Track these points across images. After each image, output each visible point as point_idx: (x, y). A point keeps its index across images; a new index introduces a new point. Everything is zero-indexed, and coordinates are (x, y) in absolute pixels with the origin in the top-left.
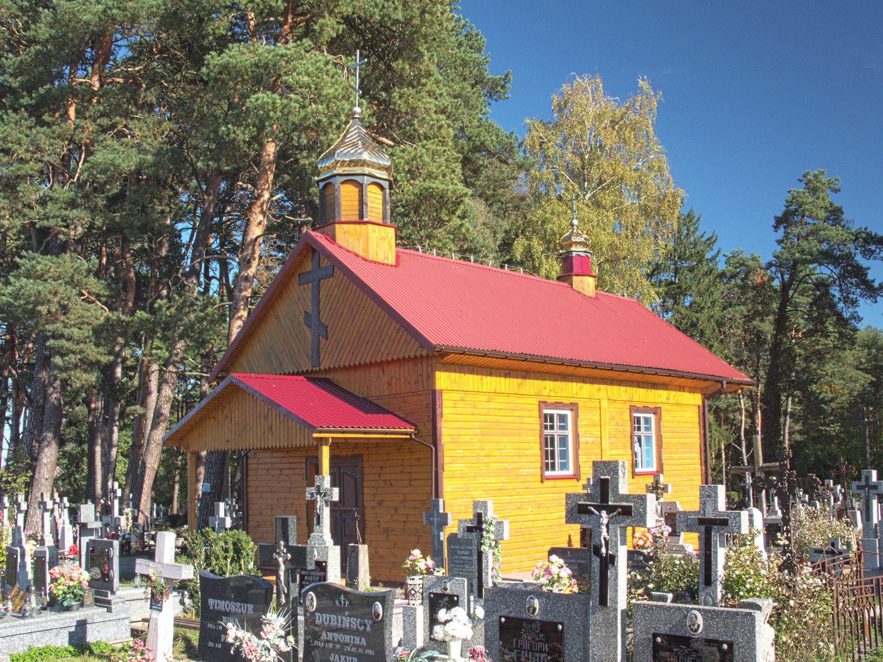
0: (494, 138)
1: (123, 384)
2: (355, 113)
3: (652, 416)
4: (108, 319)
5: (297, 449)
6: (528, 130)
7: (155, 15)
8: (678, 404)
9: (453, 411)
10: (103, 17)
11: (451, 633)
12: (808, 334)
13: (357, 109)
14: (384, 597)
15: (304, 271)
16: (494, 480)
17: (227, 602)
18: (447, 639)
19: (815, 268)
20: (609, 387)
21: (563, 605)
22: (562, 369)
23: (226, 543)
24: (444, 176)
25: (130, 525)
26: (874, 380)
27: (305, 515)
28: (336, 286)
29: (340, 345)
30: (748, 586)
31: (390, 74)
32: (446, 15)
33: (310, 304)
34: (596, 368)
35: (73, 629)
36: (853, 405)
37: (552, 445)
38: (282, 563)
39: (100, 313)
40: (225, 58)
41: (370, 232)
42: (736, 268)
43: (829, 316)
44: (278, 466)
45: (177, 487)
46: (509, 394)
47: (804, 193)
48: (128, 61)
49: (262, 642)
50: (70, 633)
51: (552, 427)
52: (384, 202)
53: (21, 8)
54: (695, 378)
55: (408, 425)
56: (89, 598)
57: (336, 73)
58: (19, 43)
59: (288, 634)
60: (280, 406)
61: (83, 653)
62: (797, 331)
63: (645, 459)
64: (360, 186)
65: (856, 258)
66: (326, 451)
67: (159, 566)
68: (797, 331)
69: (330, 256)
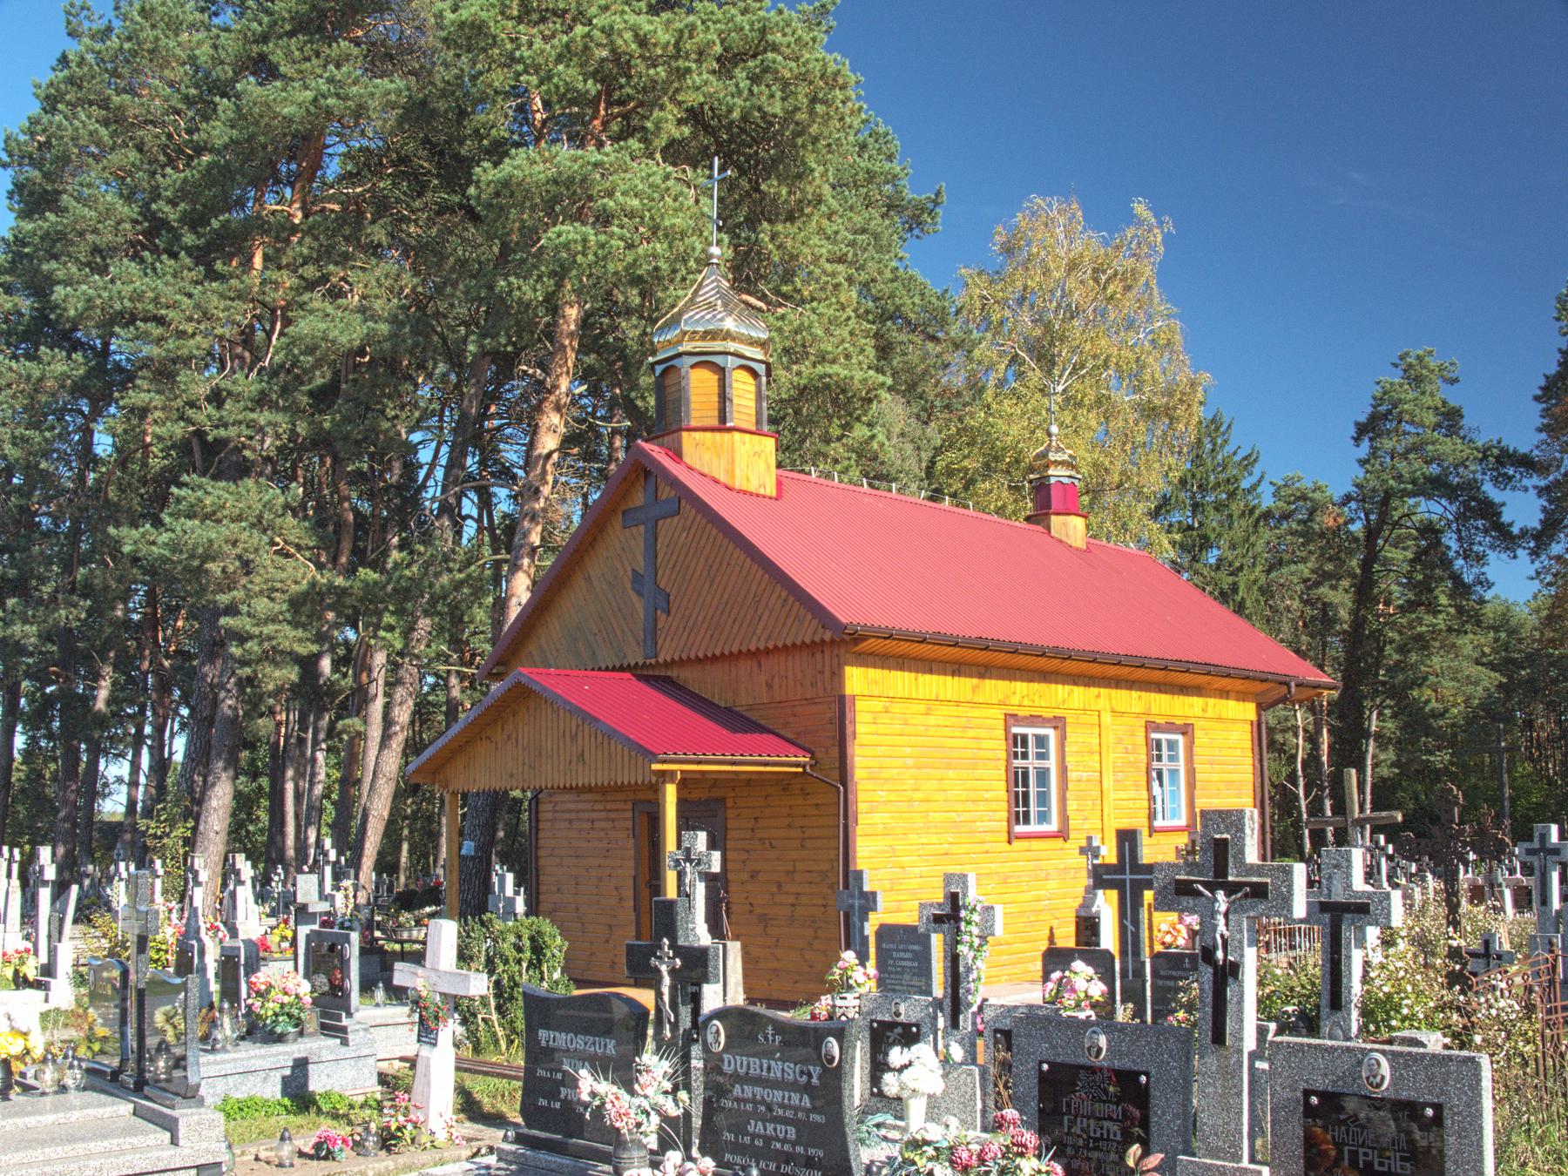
0: (917, 300)
1: (332, 683)
2: (711, 256)
3: (1180, 738)
4: (313, 584)
5: (620, 788)
6: (968, 288)
7: (394, 106)
8: (1219, 719)
9: (873, 728)
10: (312, 109)
11: (912, 1085)
12: (1409, 607)
13: (715, 250)
14: (843, 1029)
15: (631, 505)
16: (934, 839)
17: (571, 1035)
18: (905, 1095)
19: (1417, 505)
20: (1114, 692)
21: (1148, 1043)
22: (1042, 663)
23: (519, 937)
24: (848, 357)
25: (351, 906)
26: (1505, 680)
27: (631, 893)
28: (683, 529)
29: (690, 624)
30: (1405, 1011)
31: (756, 196)
32: (849, 104)
33: (641, 559)
34: (1094, 661)
35: (288, 1072)
36: (1471, 720)
37: (1026, 785)
38: (665, 974)
39: (303, 573)
40: (507, 167)
41: (737, 445)
42: (1289, 503)
43: (1442, 579)
44: (587, 815)
45: (405, 846)
46: (958, 703)
47: (1401, 386)
48: (347, 178)
49: (637, 1101)
50: (284, 1078)
51: (1025, 756)
52: (759, 397)
53: (186, 99)
54: (1247, 678)
55: (802, 752)
56: (312, 1020)
57: (681, 193)
58: (180, 151)
59: (676, 1089)
60: (596, 720)
61: (307, 1109)
62: (1387, 603)
63: (1168, 805)
64: (721, 371)
65: (1484, 488)
66: (671, 792)
67: (433, 974)
68: (1387, 603)
69: (675, 483)
